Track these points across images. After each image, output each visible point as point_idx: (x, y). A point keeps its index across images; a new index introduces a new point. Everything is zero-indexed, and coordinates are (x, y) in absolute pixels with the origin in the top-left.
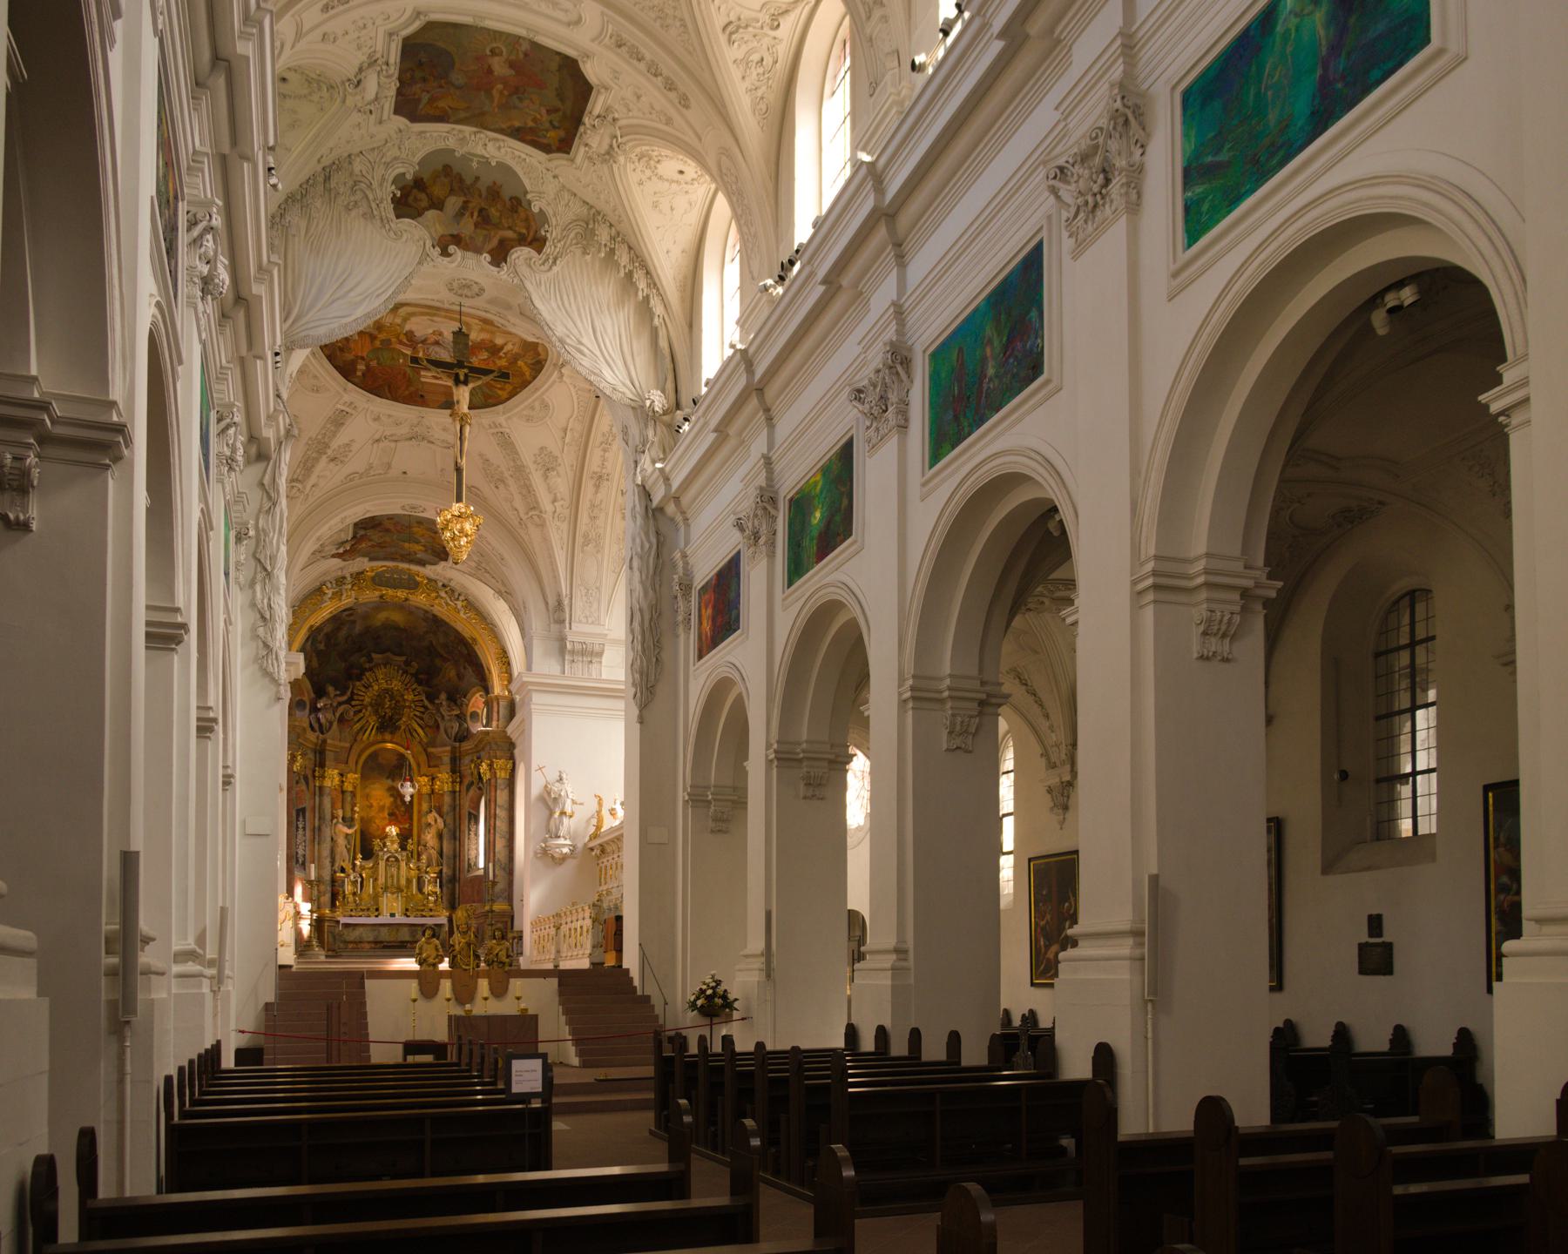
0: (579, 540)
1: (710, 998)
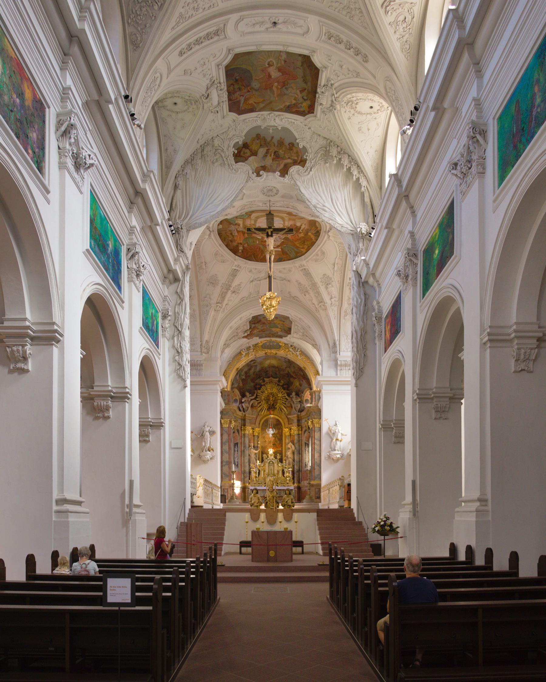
0: (343, 314)
1: (382, 527)
